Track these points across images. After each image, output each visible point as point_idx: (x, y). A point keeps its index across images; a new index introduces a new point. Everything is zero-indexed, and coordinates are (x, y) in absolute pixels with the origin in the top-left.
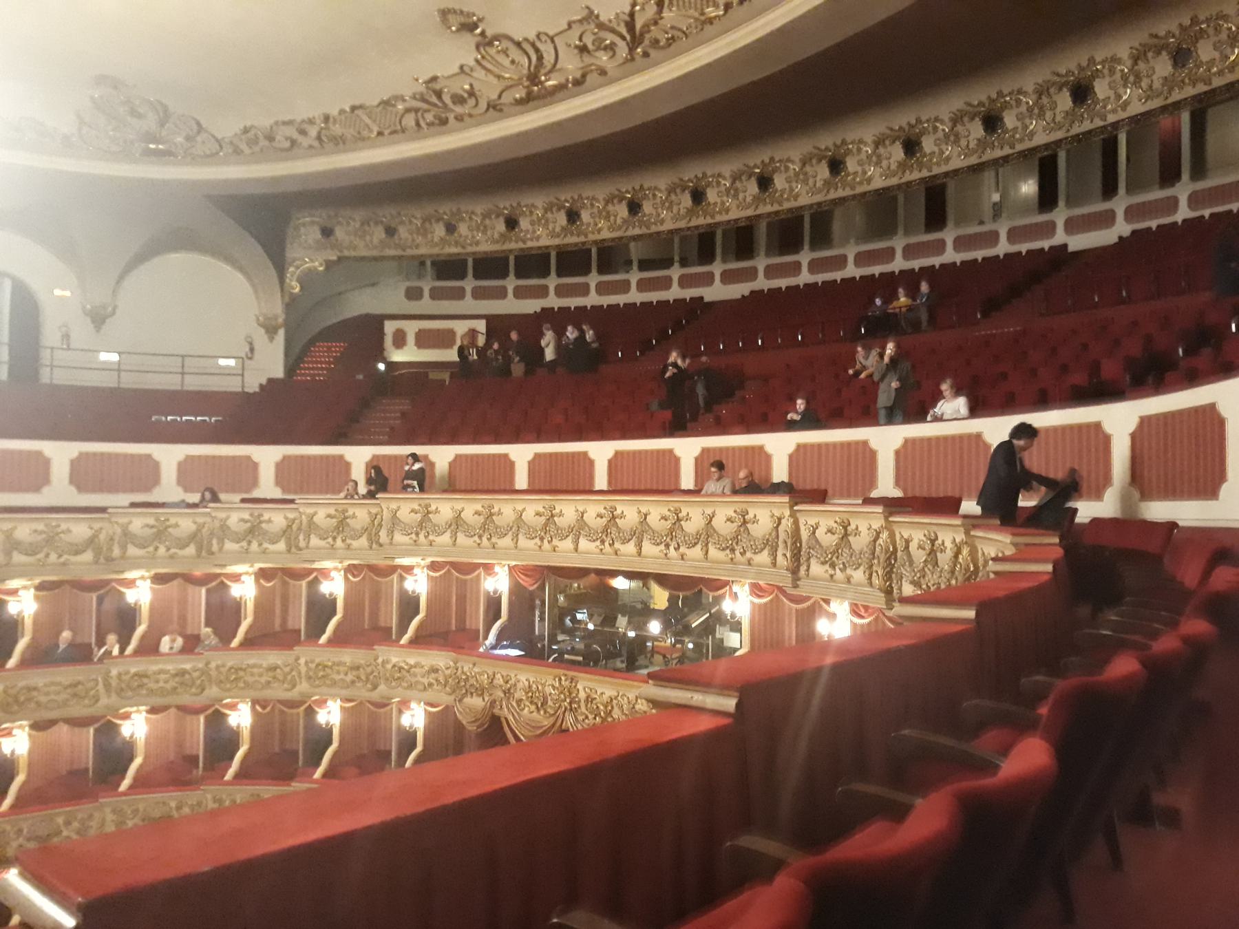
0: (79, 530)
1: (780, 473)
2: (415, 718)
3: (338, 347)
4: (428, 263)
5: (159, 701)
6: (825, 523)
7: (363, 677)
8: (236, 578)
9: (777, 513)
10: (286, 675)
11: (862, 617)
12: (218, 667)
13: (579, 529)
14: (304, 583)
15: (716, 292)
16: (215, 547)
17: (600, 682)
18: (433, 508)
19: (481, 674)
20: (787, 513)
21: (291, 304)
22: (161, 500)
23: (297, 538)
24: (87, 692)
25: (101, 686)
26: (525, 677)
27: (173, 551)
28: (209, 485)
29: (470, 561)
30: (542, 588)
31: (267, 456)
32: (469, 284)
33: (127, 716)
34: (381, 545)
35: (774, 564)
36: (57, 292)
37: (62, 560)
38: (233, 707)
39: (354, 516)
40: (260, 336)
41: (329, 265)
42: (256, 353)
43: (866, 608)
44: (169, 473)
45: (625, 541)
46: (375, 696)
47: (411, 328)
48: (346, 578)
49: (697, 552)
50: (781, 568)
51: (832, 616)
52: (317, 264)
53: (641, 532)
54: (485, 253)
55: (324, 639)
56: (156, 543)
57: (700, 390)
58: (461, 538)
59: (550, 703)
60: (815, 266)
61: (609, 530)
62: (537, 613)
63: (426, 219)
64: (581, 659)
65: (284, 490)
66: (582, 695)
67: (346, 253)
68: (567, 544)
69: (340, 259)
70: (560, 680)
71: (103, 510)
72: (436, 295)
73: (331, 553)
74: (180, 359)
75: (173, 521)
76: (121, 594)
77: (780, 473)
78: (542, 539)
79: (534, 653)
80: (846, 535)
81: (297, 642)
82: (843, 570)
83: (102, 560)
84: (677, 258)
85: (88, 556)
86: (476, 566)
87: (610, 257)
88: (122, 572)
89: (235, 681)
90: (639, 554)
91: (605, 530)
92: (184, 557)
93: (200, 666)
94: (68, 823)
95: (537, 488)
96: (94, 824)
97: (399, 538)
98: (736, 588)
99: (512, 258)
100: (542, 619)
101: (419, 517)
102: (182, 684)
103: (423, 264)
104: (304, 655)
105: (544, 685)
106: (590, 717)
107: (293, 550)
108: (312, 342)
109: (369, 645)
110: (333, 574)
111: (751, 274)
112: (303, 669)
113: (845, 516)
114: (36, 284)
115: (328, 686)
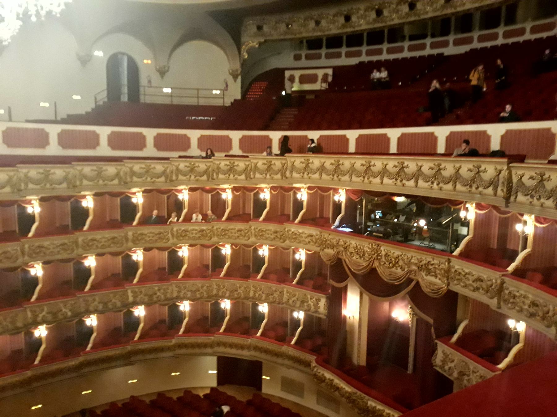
0: (159, 167)
1: (495, 145)
2: (301, 255)
3: (264, 84)
4: (305, 41)
5: (193, 242)
6: (528, 174)
7: (279, 236)
8: (224, 190)
9: (499, 167)
10: (245, 233)
11: (541, 223)
12: (217, 229)
13: (384, 173)
14: (252, 194)
15: (450, 50)
16: (215, 177)
17: (392, 247)
18: (311, 161)
19: (333, 239)
20: (505, 167)
21: (244, 64)
22: (191, 155)
23: (250, 173)
24: (165, 236)
25: (170, 235)
26: (354, 242)
27: (197, 178)
28: (211, 147)
29: (327, 186)
30: (361, 201)
31: (236, 135)
32: (323, 51)
33: (180, 248)
34: (287, 178)
35: (495, 194)
36: (145, 61)
37: (152, 180)
38: (223, 246)
39: (274, 164)
40: (230, 79)
41: (260, 44)
42: (229, 86)
43: (545, 219)
44: (194, 143)
45: (409, 180)
46: (283, 245)
47: (297, 74)
48: (271, 192)
49: (450, 186)
50: (500, 197)
51: (525, 223)
52: (255, 44)
53: (417, 175)
54: (335, 34)
55: (261, 219)
56: (190, 174)
57: (447, 102)
58: (324, 176)
59: (366, 255)
60: (507, 35)
61: (400, 173)
62: (358, 212)
63: (306, 19)
64: (382, 235)
65: (243, 152)
66: (383, 253)
67: (268, 38)
68: (377, 180)
69: (265, 41)
70: (372, 245)
71: (167, 159)
72: (308, 57)
73: (264, 181)
74: (196, 91)
75: (197, 164)
76: (177, 196)
77: (495, 145)
78: (364, 177)
79: (358, 231)
80: (542, 180)
81: (250, 220)
82: (538, 199)
83: (168, 181)
84: (429, 33)
85: (162, 179)
86: (330, 189)
87: (395, 34)
88: (176, 186)
89: (224, 234)
90: (416, 186)
91: (398, 173)
92: (202, 181)
93: (210, 228)
94: (159, 290)
95: (359, 151)
96: (169, 291)
97: (295, 175)
98: (468, 205)
99: (365, 34)
100: (361, 214)
101: (304, 165)
102: (202, 235)
103: (301, 42)
104: (254, 226)
105: (364, 247)
106: (387, 263)
107: (248, 179)
108: (250, 84)
109: (281, 222)
110: (265, 190)
111: (469, 41)
112: (253, 232)
113: (542, 170)
114: (136, 57)
115: (263, 239)
